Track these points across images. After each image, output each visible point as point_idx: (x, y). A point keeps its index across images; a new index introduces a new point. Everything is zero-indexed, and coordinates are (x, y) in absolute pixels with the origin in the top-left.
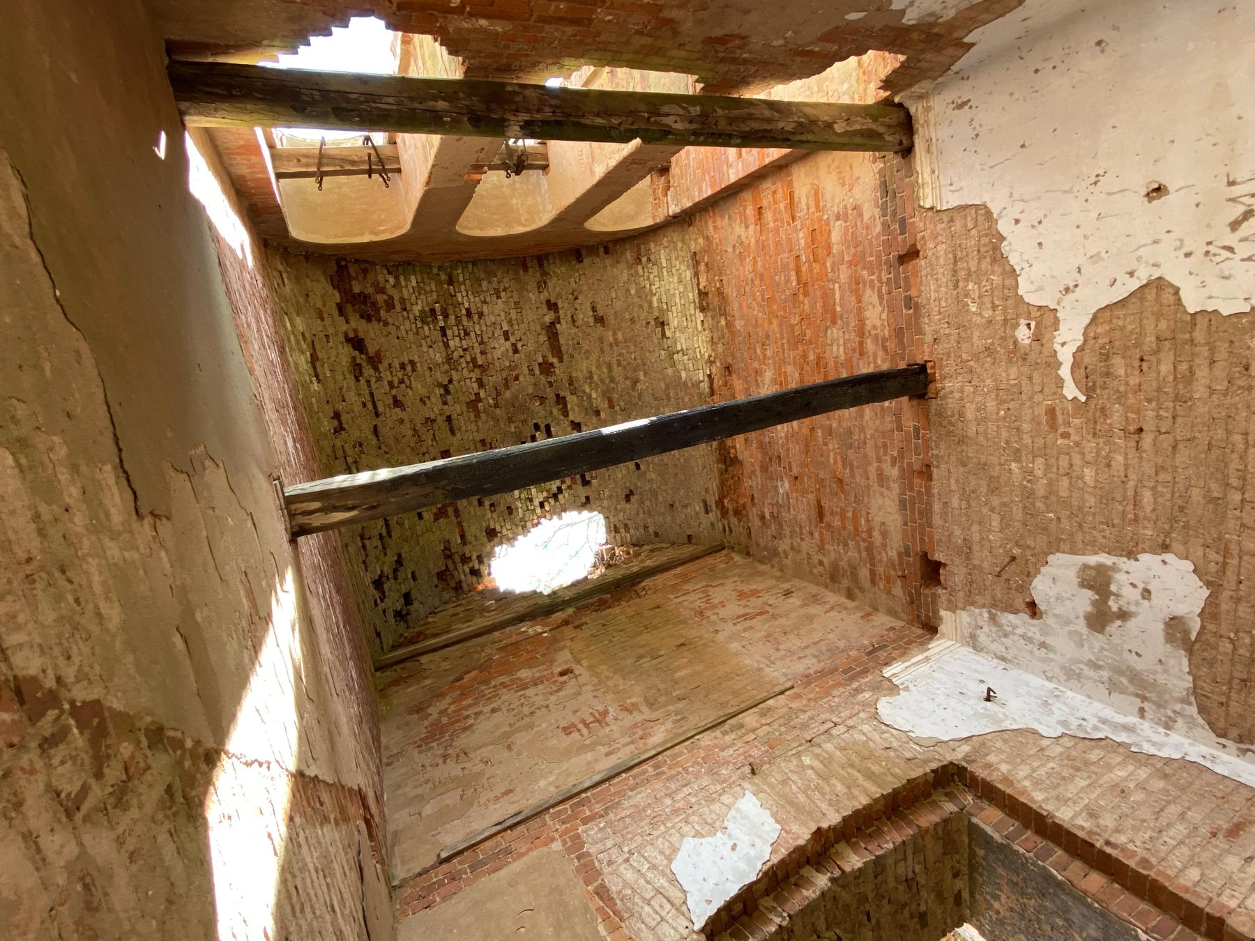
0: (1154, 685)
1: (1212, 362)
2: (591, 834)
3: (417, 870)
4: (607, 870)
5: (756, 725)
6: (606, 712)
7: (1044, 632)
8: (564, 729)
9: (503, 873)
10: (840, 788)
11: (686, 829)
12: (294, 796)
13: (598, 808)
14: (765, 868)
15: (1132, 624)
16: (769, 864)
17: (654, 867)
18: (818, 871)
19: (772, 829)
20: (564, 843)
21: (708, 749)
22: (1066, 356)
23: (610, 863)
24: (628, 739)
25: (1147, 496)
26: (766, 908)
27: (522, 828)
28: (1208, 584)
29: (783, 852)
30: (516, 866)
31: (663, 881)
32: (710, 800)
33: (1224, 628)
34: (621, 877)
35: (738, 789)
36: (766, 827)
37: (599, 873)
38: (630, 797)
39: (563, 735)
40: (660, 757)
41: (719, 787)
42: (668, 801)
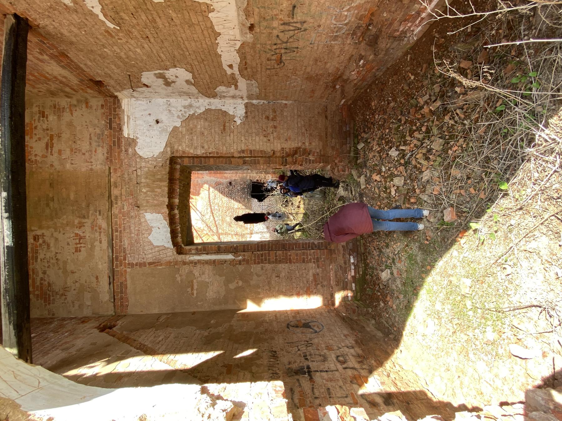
0: (189, 93)
1: (160, 17)
2: (130, 259)
3: (113, 308)
4: (145, 260)
5: (119, 192)
6: (77, 235)
7: (154, 89)
8: (76, 251)
9: (128, 286)
10: (159, 190)
11: (145, 235)
13: (122, 254)
15: (176, 83)
17: (152, 249)
19: (160, 216)
20: (129, 268)
21: (120, 212)
22: (97, 10)
23: (144, 259)
24: (98, 233)
25: (162, 55)
27: (115, 277)
28: (191, 72)
29: (167, 218)
30: (129, 282)
31: (157, 249)
32: (140, 224)
33: (199, 80)
34: (149, 258)
35: (141, 215)
36: (159, 217)
37: (145, 263)
38: (124, 245)
39: (79, 253)
40: (114, 228)
41: (137, 219)
42: (133, 235)
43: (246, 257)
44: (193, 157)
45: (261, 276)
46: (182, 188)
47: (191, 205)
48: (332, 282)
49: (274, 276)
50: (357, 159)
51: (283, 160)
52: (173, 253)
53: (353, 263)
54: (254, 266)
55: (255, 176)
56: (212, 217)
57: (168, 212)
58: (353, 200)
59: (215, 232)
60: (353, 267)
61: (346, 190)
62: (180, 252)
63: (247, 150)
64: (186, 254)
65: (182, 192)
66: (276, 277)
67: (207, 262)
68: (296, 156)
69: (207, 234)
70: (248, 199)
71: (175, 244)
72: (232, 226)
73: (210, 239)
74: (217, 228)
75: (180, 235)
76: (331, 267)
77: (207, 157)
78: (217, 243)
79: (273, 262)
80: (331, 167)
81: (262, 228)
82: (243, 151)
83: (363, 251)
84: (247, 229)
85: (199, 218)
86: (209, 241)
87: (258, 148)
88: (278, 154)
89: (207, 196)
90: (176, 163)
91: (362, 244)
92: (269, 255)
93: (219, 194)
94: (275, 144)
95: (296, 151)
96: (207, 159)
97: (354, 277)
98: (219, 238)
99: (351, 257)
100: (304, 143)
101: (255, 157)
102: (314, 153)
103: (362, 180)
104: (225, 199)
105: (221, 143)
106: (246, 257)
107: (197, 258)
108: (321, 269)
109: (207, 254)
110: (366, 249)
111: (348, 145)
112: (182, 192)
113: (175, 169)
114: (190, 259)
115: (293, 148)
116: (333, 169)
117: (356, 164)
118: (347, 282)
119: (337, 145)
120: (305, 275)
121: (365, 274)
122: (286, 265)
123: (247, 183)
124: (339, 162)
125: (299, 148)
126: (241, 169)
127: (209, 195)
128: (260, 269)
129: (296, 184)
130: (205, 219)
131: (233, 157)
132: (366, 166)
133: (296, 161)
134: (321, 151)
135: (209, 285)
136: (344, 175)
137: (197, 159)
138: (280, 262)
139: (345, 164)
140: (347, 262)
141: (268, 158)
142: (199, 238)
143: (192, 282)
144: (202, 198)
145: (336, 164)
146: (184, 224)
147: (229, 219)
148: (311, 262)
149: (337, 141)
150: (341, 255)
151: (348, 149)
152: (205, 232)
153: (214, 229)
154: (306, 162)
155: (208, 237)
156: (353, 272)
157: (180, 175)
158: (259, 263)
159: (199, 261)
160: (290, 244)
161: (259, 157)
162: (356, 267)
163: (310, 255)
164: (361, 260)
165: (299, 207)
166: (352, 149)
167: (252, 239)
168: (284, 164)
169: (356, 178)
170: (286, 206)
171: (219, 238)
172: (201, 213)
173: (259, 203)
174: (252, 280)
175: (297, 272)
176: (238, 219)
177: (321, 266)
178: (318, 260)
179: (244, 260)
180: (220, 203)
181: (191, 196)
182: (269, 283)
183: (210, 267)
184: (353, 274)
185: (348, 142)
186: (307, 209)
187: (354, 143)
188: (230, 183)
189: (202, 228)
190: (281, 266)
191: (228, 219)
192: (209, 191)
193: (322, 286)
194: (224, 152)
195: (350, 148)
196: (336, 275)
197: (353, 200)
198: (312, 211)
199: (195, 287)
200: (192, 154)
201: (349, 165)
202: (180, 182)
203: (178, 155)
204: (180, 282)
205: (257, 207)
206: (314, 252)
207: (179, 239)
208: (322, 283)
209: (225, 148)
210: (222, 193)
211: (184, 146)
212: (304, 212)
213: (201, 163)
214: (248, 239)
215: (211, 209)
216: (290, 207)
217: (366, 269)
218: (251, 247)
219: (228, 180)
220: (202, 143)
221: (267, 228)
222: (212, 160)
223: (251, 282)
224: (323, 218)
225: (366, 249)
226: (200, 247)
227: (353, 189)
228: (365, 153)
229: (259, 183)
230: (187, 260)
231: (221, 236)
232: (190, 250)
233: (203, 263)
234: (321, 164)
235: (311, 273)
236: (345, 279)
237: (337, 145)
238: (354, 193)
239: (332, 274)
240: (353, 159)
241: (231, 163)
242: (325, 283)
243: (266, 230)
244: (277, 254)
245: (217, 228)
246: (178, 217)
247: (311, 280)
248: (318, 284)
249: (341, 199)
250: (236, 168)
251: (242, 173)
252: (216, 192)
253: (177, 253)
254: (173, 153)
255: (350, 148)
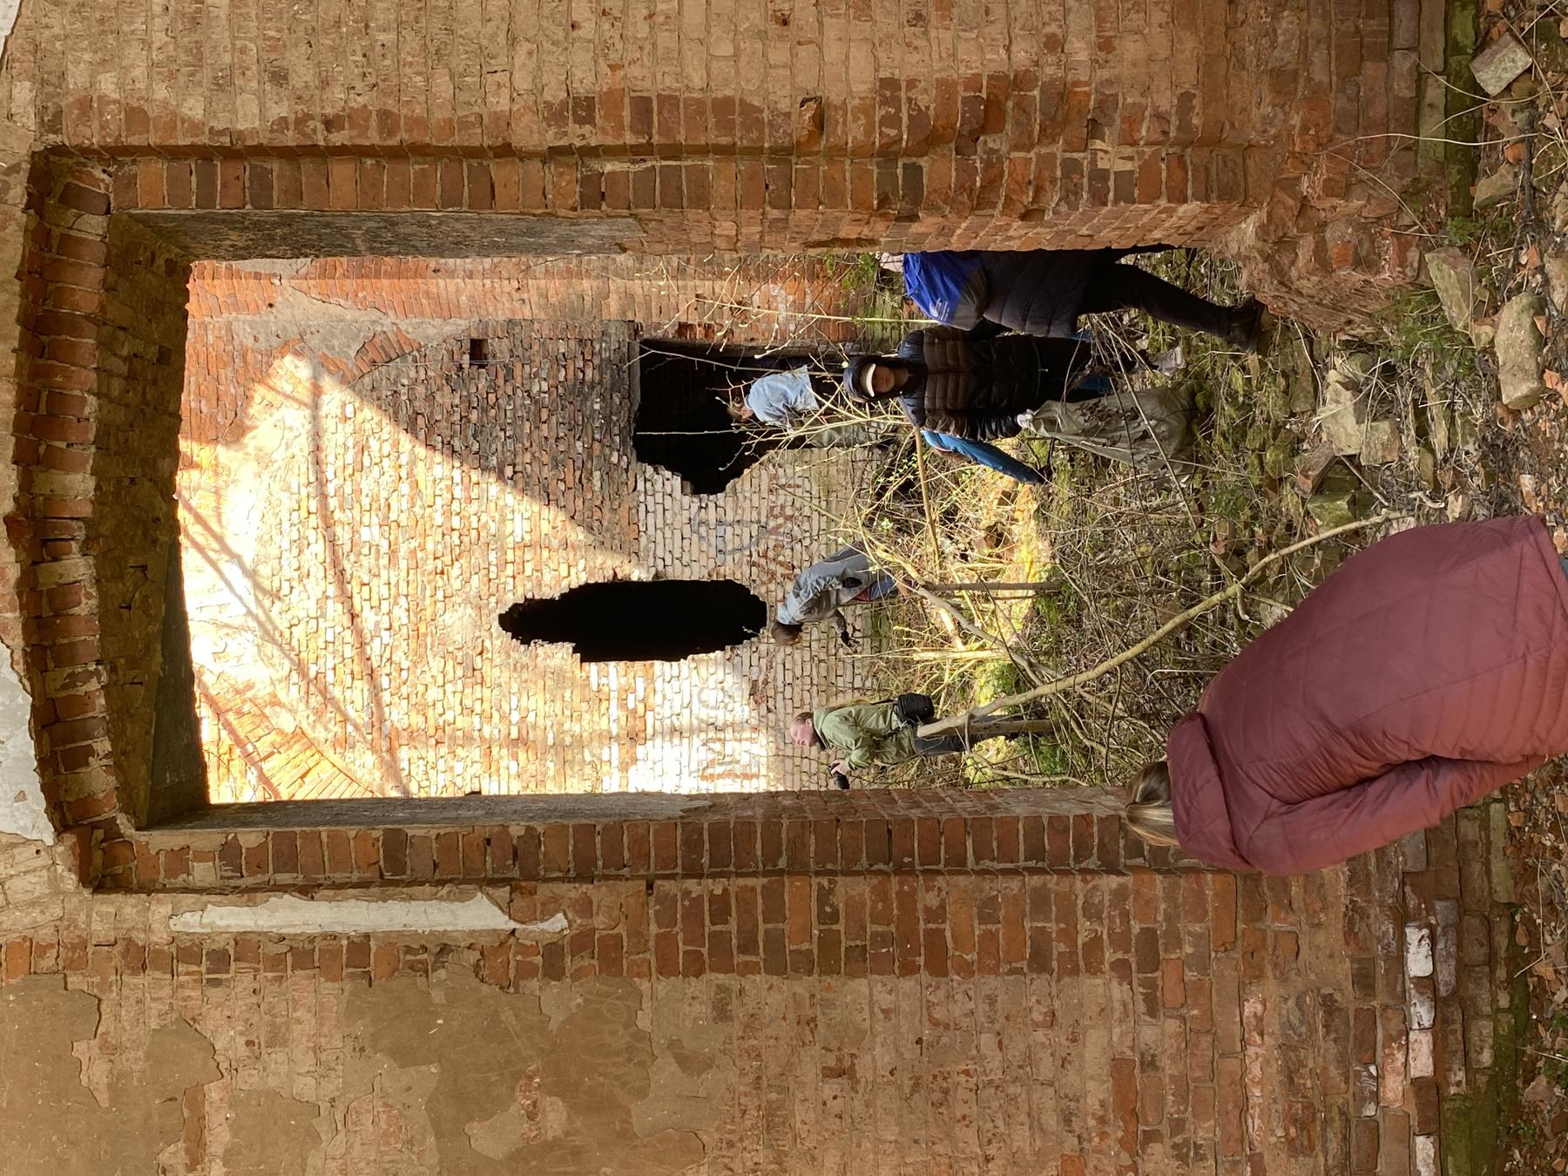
12: (567, 814)
14: (20, 667)
16: (18, 655)
18: (55, 559)
26: (64, 687)
43: (599, 921)
44: (205, 154)
45: (708, 1064)
46: (116, 386)
47: (182, 514)
48: (1255, 1124)
49: (809, 1070)
50: (1471, 167)
51: (887, 177)
52: (54, 881)
53: (1428, 984)
54: (663, 986)
55: (668, 292)
56: (335, 610)
57: (14, 573)
58: (1437, 492)
59: (362, 718)
60: (1422, 1013)
61: (1377, 406)
62: (103, 870)
63: (612, 99)
64: (148, 888)
65: (120, 416)
66: (830, 1073)
67: (303, 954)
68: (993, 142)
69: (299, 734)
70: (609, 471)
71: (67, 811)
72: (492, 673)
73: (325, 770)
74: (376, 691)
75: (103, 745)
76: (1252, 1007)
77: (312, 151)
78: (379, 805)
79: (804, 964)
80: (1262, 231)
81: (711, 696)
82: (583, 109)
83: (1503, 889)
84: (600, 698)
85: (235, 614)
86: (306, 792)
87: (698, 80)
88: (853, 132)
89: (303, 445)
90: (74, 198)
91: (1499, 839)
92: (775, 911)
93: (388, 427)
94: (833, 52)
95: (990, 107)
96: (307, 166)
97: (1428, 1091)
98: (392, 768)
99: (1413, 934)
100: (1054, 44)
101: (673, 151)
102: (1132, 121)
103: (1510, 333)
104: (436, 471)
105: (412, 43)
106: (599, 921)
107: (226, 918)
108: (1172, 1025)
109: (307, 891)
110: (1526, 874)
111: (1403, 63)
112: (120, 416)
113: (69, 244)
114: (177, 925)
115: (973, 83)
116: (1277, 245)
117: (1465, 210)
118: (1373, 1127)
119: (1318, 57)
120: (1046, 1069)
121: (1515, 1064)
122: (907, 984)
123: (604, 350)
124: (1330, 189)
125: (1020, 81)
126: (566, 244)
127: (317, 435)
128: (703, 1009)
129: (1008, 350)
130: (282, 624)
131: (505, 151)
132: (1539, 224)
133: (991, 184)
134: (1185, 99)
135: (323, 1128)
136: (1362, 292)
137: (235, 168)
138: (860, 961)
139: (1371, 212)
140: (1376, 974)
141: (766, 163)
142: (237, 765)
143: (195, 1097)
144: (264, 460)
145: (1304, 203)
146: (133, 663)
147: (468, 622)
148: (1094, 969)
149: (1316, 25)
150: (1334, 921)
151: (1404, 89)
152: (286, 723)
153: (355, 698)
154: (1070, 196)
155: (305, 759)
156: (1422, 1044)
157: (109, 288)
158: (695, 967)
159: (246, 947)
160: (933, 827)
161: (703, 151)
162: (1452, 1007)
163: (1093, 912)
164: (1491, 960)
165: (997, 536)
166: (1435, 92)
167: (642, 780)
168: (896, 208)
169: (1458, 313)
170: (902, 528)
171: (392, 768)
172: (251, 574)
173: (691, 503)
174: (642, 1093)
175: (987, 1041)
176: (530, 621)
177: (1171, 993)
178: (1150, 952)
179: (581, 941)
180: (399, 504)
181: (184, 445)
182: (773, 1120)
183: (327, 987)
184: (1422, 1065)
185: (1402, 37)
186: (1065, 556)
187: (1452, 47)
188: (477, 350)
189: (262, 692)
190: (861, 994)
191: (458, 622)
192: (315, 406)
193: (1181, 1153)
194: (440, 115)
195: (1420, 80)
196: (1290, 1076)
197: (1437, 492)
198: (1104, 571)
199: (219, 1136)
200: (196, 128)
201: (1408, 217)
202: (106, 345)
203: (93, 136)
204: (103, 1098)
205: (678, 533)
206: (1120, 895)
207: (99, 778)
208: (1178, 1126)
209: (443, 86)
210: (411, 429)
211: (139, 72)
212: (1038, 575)
213: (262, 197)
214: (611, 784)
215: (332, 542)
216: (932, 540)
217: (1524, 1030)
218: (639, 842)
219: (461, 326)
220: (276, 46)
221: (755, 692)
222: (342, 172)
223: (636, 1107)
224: (1188, 628)
225: (1526, 874)
226: (250, 838)
227: (1434, 404)
228: (1532, 124)
229: (698, 350)
230: (159, 937)
231: (404, 753)
232: (180, 861)
233: (276, 962)
234: (1192, 207)
235: (1095, 1048)
236: (1360, 1100)
237: (1318, 57)
238: (1439, 438)
239: (1259, 1063)
240: (1442, 169)
241: (489, 196)
242: (1204, 1132)
243: (742, 710)
244: (839, 900)
245: (376, 691)
246: (86, 606)
247: (1092, 1103)
248: (1151, 1137)
249: (1342, 478)
250: (528, 236)
251: (569, 274)
252: (369, 414)
253: (85, 880)
254: (51, 122)
255: (1420, 80)
